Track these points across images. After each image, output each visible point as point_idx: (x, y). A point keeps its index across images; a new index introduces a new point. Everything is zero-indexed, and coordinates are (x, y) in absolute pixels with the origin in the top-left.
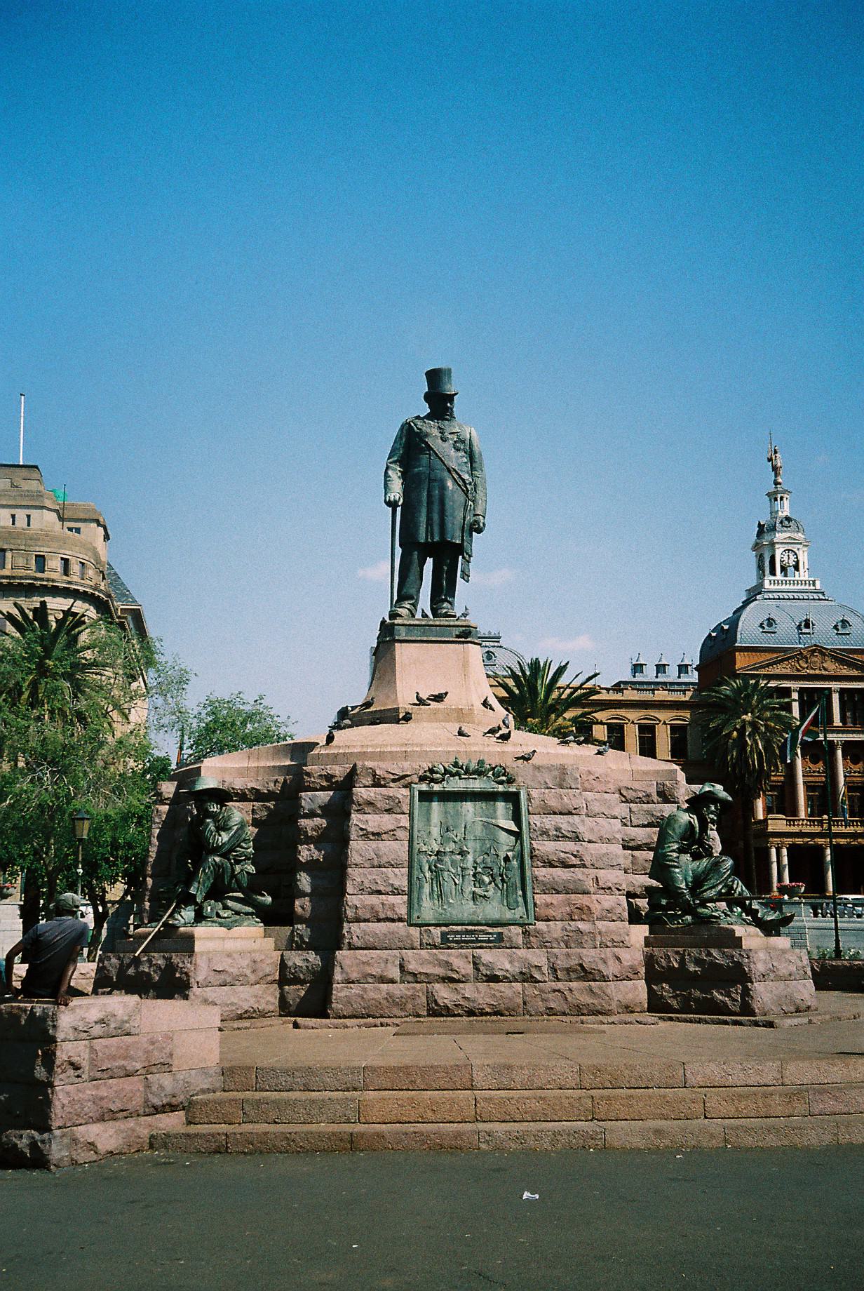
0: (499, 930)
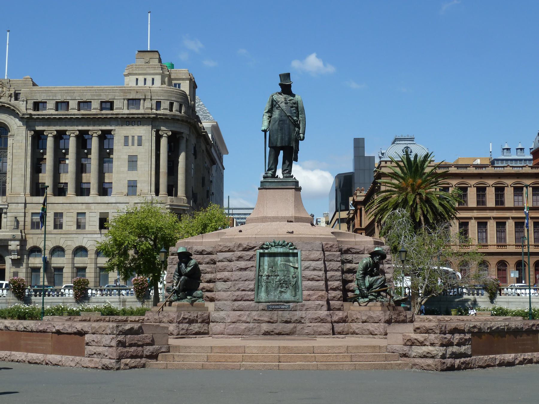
0: (288, 304)
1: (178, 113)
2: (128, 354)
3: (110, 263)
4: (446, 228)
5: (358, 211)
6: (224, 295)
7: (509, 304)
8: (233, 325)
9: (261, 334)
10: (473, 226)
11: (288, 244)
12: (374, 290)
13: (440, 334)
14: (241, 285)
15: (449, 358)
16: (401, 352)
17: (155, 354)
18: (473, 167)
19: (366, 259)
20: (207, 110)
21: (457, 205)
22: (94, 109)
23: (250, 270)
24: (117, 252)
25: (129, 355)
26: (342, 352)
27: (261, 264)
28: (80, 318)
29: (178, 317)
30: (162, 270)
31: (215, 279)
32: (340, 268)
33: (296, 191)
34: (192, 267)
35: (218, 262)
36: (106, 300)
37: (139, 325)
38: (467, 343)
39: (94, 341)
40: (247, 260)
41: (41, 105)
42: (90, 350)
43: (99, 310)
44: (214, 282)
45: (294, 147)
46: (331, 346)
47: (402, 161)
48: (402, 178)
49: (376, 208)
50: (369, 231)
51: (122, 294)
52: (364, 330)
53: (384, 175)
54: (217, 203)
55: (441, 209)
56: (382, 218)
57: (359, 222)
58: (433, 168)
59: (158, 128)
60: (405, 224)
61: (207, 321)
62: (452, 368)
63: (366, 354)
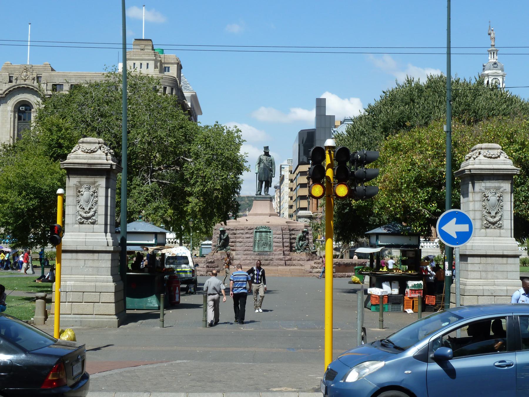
14: (247, 244)
19: (300, 234)
20: (187, 81)
29: (221, 257)
41: (58, 87)
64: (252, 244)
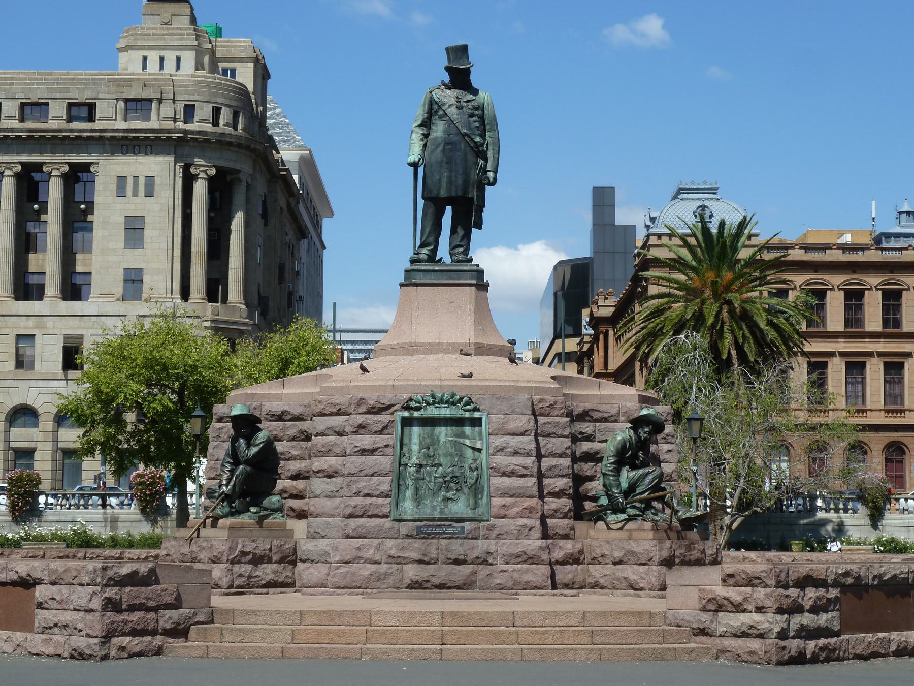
0: (461, 525)
1: (229, 130)
2: (126, 627)
3: (86, 438)
4: (783, 372)
5: (601, 337)
6: (327, 504)
7: (909, 531)
8: (345, 567)
9: (404, 586)
10: (836, 370)
11: (461, 399)
12: (638, 497)
13: (776, 587)
14: (362, 484)
15: (793, 638)
16: (695, 626)
17: (182, 626)
18: (839, 248)
19: (622, 433)
21: (803, 327)
22: (54, 118)
23: (382, 453)
24: (102, 416)
25: (128, 628)
26: (573, 624)
27: (406, 440)
28: (22, 552)
29: (231, 549)
30: (197, 454)
31: (308, 472)
32: (568, 451)
33: (479, 290)
34: (261, 445)
35: (315, 436)
36: (77, 516)
37: (150, 565)
38: (832, 607)
39: (54, 599)
40: (376, 432)
42: (45, 619)
43: (62, 538)
44: (307, 478)
45: (475, 198)
46: (549, 612)
47: (693, 235)
48: (693, 269)
49: (639, 331)
50: (624, 375)
51: (110, 505)
52: (617, 579)
53: (657, 263)
54: (309, 315)
55: (771, 334)
56: (651, 351)
57: (602, 360)
58: (756, 249)
59: (189, 161)
60: (699, 363)
61: (291, 559)
62: (799, 659)
63: (624, 628)
64: (385, 484)
